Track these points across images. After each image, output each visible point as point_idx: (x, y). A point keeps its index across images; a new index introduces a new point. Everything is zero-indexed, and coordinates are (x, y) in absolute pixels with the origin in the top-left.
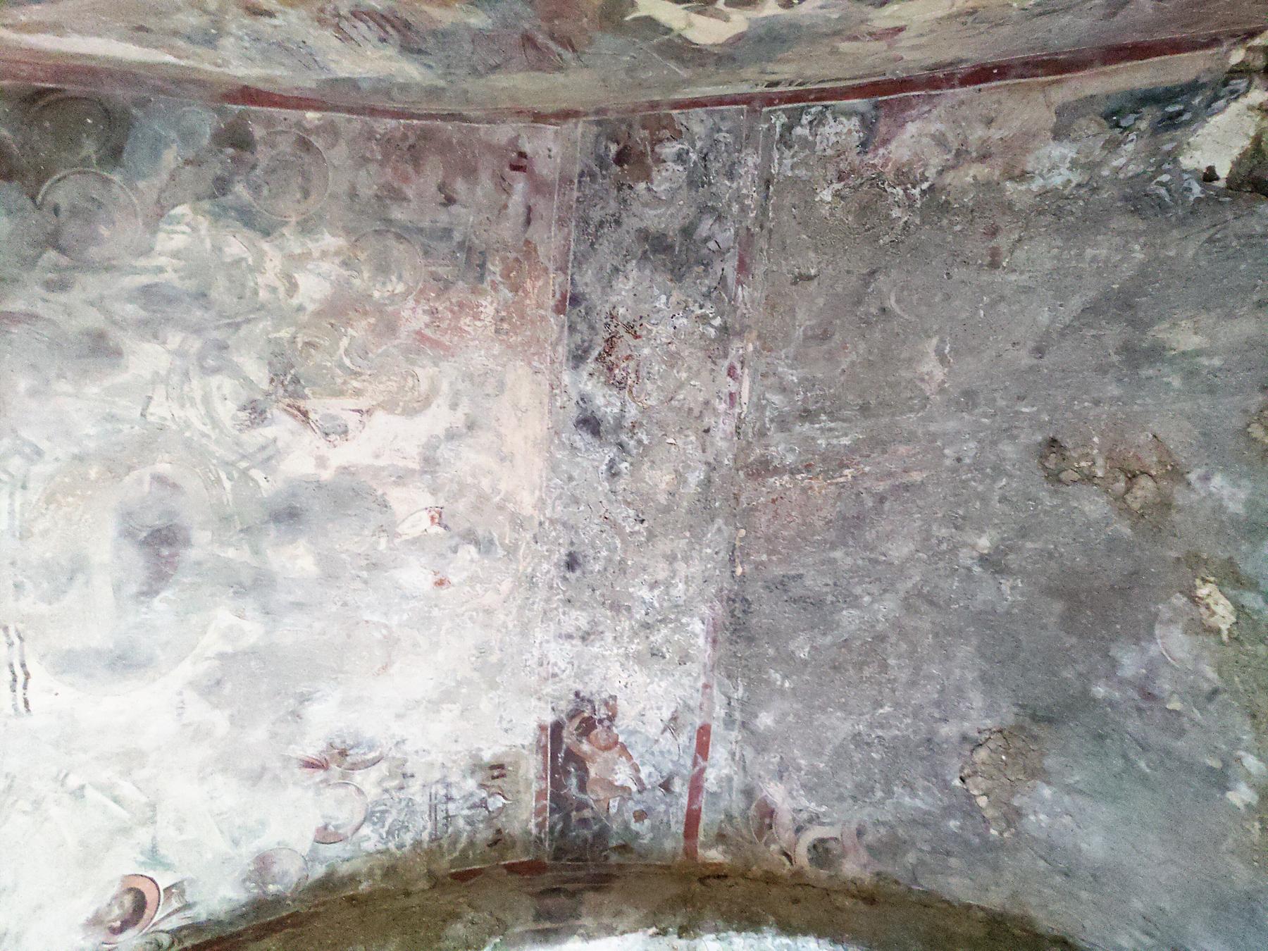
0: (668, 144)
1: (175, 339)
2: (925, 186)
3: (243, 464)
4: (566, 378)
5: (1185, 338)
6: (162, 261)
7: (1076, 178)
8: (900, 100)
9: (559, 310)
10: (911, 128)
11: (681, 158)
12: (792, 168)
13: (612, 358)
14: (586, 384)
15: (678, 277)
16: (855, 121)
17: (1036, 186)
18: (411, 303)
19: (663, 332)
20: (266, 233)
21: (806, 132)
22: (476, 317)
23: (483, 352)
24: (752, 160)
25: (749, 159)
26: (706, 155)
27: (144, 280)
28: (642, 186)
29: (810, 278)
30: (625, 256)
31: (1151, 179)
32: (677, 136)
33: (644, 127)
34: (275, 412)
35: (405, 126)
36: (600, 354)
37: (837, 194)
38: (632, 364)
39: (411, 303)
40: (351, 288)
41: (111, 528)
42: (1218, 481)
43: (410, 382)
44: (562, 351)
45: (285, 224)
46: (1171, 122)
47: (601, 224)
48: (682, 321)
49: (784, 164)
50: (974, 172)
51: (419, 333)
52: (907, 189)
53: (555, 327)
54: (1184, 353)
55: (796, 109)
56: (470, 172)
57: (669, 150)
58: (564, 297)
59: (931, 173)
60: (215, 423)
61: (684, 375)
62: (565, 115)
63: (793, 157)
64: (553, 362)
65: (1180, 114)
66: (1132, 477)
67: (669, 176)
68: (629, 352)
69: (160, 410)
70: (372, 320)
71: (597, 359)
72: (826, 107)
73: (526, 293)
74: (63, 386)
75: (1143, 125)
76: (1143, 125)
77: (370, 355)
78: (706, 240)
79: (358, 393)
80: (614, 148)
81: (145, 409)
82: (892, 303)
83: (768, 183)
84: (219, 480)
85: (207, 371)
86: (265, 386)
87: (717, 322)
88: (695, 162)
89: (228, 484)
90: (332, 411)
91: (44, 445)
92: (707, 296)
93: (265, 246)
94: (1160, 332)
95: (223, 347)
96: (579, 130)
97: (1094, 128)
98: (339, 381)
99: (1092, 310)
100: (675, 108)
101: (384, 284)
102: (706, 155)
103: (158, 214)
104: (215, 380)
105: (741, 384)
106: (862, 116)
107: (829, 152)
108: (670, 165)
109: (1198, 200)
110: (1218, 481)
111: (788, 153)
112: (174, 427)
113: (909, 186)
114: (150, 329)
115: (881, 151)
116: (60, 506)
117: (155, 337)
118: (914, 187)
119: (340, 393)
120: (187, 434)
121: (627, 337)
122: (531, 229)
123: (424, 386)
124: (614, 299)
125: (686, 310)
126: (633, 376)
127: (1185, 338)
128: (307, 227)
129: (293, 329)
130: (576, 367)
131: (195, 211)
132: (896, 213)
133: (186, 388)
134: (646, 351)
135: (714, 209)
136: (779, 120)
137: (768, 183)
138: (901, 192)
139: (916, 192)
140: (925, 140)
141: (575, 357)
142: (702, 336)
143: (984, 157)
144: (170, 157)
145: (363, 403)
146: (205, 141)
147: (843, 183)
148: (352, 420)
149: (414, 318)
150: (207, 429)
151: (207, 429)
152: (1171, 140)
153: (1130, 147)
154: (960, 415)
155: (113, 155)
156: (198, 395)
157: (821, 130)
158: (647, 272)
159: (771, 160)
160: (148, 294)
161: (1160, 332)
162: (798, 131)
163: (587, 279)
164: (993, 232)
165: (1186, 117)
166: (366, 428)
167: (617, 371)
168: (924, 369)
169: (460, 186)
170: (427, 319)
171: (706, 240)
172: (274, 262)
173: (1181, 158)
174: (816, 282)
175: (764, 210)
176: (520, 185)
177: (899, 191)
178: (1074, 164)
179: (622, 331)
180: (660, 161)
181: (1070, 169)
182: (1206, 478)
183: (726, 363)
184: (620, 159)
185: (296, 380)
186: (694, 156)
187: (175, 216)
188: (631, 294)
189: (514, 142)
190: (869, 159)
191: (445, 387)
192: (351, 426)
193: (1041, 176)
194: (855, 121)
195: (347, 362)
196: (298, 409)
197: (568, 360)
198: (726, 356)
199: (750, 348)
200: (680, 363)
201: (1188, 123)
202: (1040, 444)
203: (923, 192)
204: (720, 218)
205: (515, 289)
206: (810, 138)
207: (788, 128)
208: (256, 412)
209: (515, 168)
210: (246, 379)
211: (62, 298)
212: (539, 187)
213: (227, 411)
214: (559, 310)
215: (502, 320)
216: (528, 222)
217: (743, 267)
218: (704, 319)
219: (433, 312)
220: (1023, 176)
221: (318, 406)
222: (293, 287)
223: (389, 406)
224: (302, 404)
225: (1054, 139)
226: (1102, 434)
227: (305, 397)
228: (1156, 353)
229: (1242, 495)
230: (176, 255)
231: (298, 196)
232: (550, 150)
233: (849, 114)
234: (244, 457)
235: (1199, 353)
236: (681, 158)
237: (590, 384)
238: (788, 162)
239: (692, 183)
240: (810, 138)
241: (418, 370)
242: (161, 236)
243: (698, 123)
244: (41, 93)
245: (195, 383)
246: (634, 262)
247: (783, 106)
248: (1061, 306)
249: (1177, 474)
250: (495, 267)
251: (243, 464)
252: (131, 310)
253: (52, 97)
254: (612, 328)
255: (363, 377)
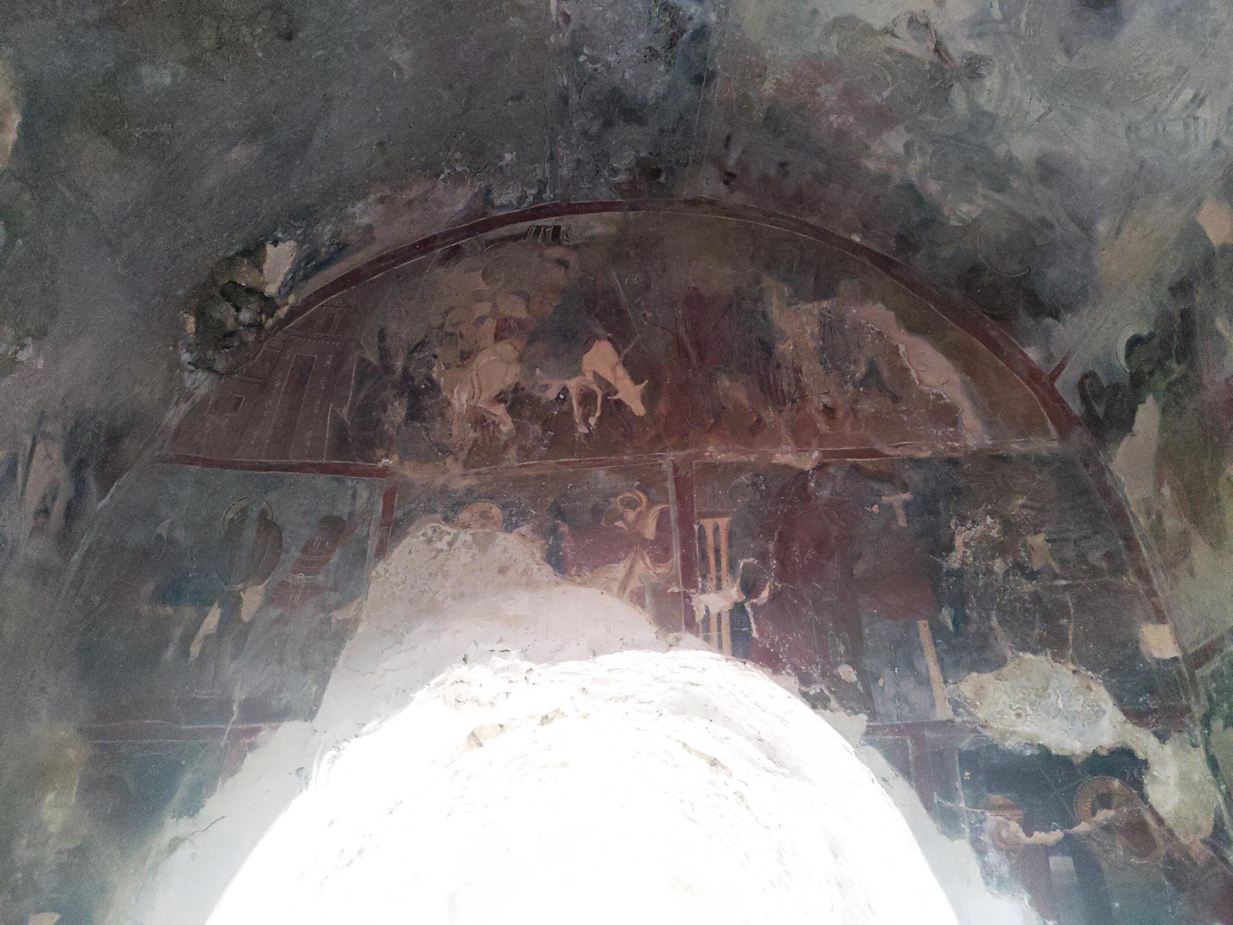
0: (623, 180)
1: (1000, 150)
2: (442, 176)
3: (1002, 27)
4: (713, 17)
5: (239, 154)
6: (980, 201)
7: (350, 210)
8: (471, 220)
9: (712, 75)
10: (461, 206)
11: (615, 172)
12: (535, 168)
13: (672, 31)
14: (696, 10)
15: (615, 92)
16: (497, 202)
17: (372, 198)
18: (828, 104)
19: (627, 51)
20: (911, 187)
21: (529, 192)
22: (779, 82)
23: (780, 53)
24: (564, 172)
25: (566, 172)
26: (596, 175)
27: (997, 196)
28: (643, 154)
29: (512, 99)
30: (657, 108)
31: (307, 226)
32: (618, 186)
33: (640, 191)
34: (958, 61)
35: (800, 216)
36: (682, 35)
37: (501, 158)
38: (654, 25)
39: (828, 104)
40: (867, 129)
41: (1126, 34)
42: (167, 80)
43: (844, 45)
44: (714, 41)
45: (899, 187)
46: (309, 258)
47: (674, 131)
48: (612, 58)
49: (542, 170)
50: (413, 193)
51: (828, 81)
52: (453, 171)
53: (717, 61)
54: (236, 144)
55: (537, 203)
56: (764, 179)
57: (622, 177)
58: (708, 85)
59: (441, 185)
60: (1006, 76)
61: (609, 15)
62: (695, 203)
63: (536, 175)
64: (723, 33)
65: (307, 264)
66: (221, 44)
67: (624, 160)
68: (656, 35)
69: (1037, 108)
70: (860, 102)
71: (685, 31)
72: (517, 208)
73: (737, 90)
74: (1084, 163)
75: (324, 250)
76: (324, 250)
77: (870, 76)
78: (593, 119)
79: (890, 50)
80: (662, 179)
81: (1046, 114)
82: (446, 95)
83: (552, 157)
84: (1028, 24)
85: (992, 116)
86: (957, 87)
87: (582, 58)
88: (605, 169)
89: (1023, 17)
90: (914, 43)
91: (1121, 131)
92: (592, 78)
93: (915, 179)
94: (257, 150)
95: (973, 128)
96: (686, 193)
97: (352, 238)
98: (900, 65)
99: (305, 143)
100: (619, 202)
101: (844, 124)
102: (596, 175)
103: (970, 226)
104: (989, 108)
105: (558, 8)
106: (493, 207)
107: (511, 183)
108: (623, 168)
109: (276, 230)
110: (167, 80)
111: (540, 176)
112: (1035, 89)
113: (453, 174)
114: (1011, 164)
115: (476, 190)
116: (1146, 76)
117: (1011, 158)
118: (449, 174)
119: (905, 55)
120: (1029, 77)
121: (658, 48)
122: (727, 133)
123: (834, 38)
124: (668, 78)
125: (607, 65)
126: (654, 15)
127: (239, 154)
128: (886, 178)
129: (920, 117)
130: (704, 26)
131: (948, 218)
132: (458, 155)
133: (1011, 114)
134: (642, 36)
135: (590, 139)
136: (548, 194)
137: (552, 157)
138: (457, 168)
139: (447, 171)
140: (449, 202)
141: (704, 35)
142: (593, 47)
143: (410, 203)
144: (947, 252)
145: (888, 41)
146: (923, 251)
147: (499, 165)
148: (902, 30)
149: (828, 93)
150: (1014, 74)
151: (1014, 74)
152: (304, 251)
153: (326, 238)
154: (369, 27)
155: (976, 269)
156: (1006, 103)
157: (519, 194)
158: (640, 97)
159: (551, 172)
160: (1000, 186)
161: (257, 150)
162: (534, 191)
163: (688, 94)
164: (388, 164)
165: (302, 264)
166: (892, 18)
167: (668, 20)
168: (407, 55)
169: (772, 172)
170: (819, 90)
171: (593, 119)
172: (915, 166)
173: (296, 244)
174: (507, 97)
175: (553, 141)
176: (731, 163)
177: (458, 169)
178: (354, 216)
179: (662, 52)
180: (630, 170)
181: (354, 214)
182: (175, 76)
183: (572, 26)
184: (658, 172)
185: (933, 79)
186: (606, 173)
187: (959, 222)
188: (653, 80)
189: (732, 191)
190: (482, 184)
191: (818, 31)
192: (904, 24)
193: (370, 204)
194: (497, 202)
195: (889, 78)
196: (940, 56)
197: (710, 33)
198: (573, 32)
199: (552, 39)
200: (612, 26)
201: (301, 261)
202: (298, 31)
203: (442, 172)
204: (585, 133)
205: (745, 96)
206: (526, 189)
207: (540, 192)
208: (974, 68)
209: (733, 176)
210: (968, 96)
211: (1047, 214)
212: (718, 161)
213: (992, 81)
214: (712, 75)
215: (760, 76)
216: (728, 138)
217: (565, 99)
218: (593, 60)
219: (813, 93)
220: (382, 200)
221: (921, 51)
222: (908, 147)
223: (868, 30)
224: (936, 59)
225: (370, 225)
226: (258, 61)
227: (931, 63)
228: (252, 135)
229: (147, 82)
230: (970, 201)
231: (881, 199)
232: (707, 183)
233: (502, 206)
234: (999, 34)
235: (228, 150)
236: (615, 172)
237: (692, 10)
238: (539, 171)
239: (607, 156)
240: (526, 189)
241: (836, 52)
242: (974, 216)
243: (604, 194)
244: (993, 317)
245: (1002, 114)
246: (650, 103)
247: (547, 203)
248: (327, 136)
249: (193, 62)
250: (758, 114)
251: (1002, 27)
252: (1016, 183)
253: (989, 312)
254: (670, 55)
255: (881, 61)
